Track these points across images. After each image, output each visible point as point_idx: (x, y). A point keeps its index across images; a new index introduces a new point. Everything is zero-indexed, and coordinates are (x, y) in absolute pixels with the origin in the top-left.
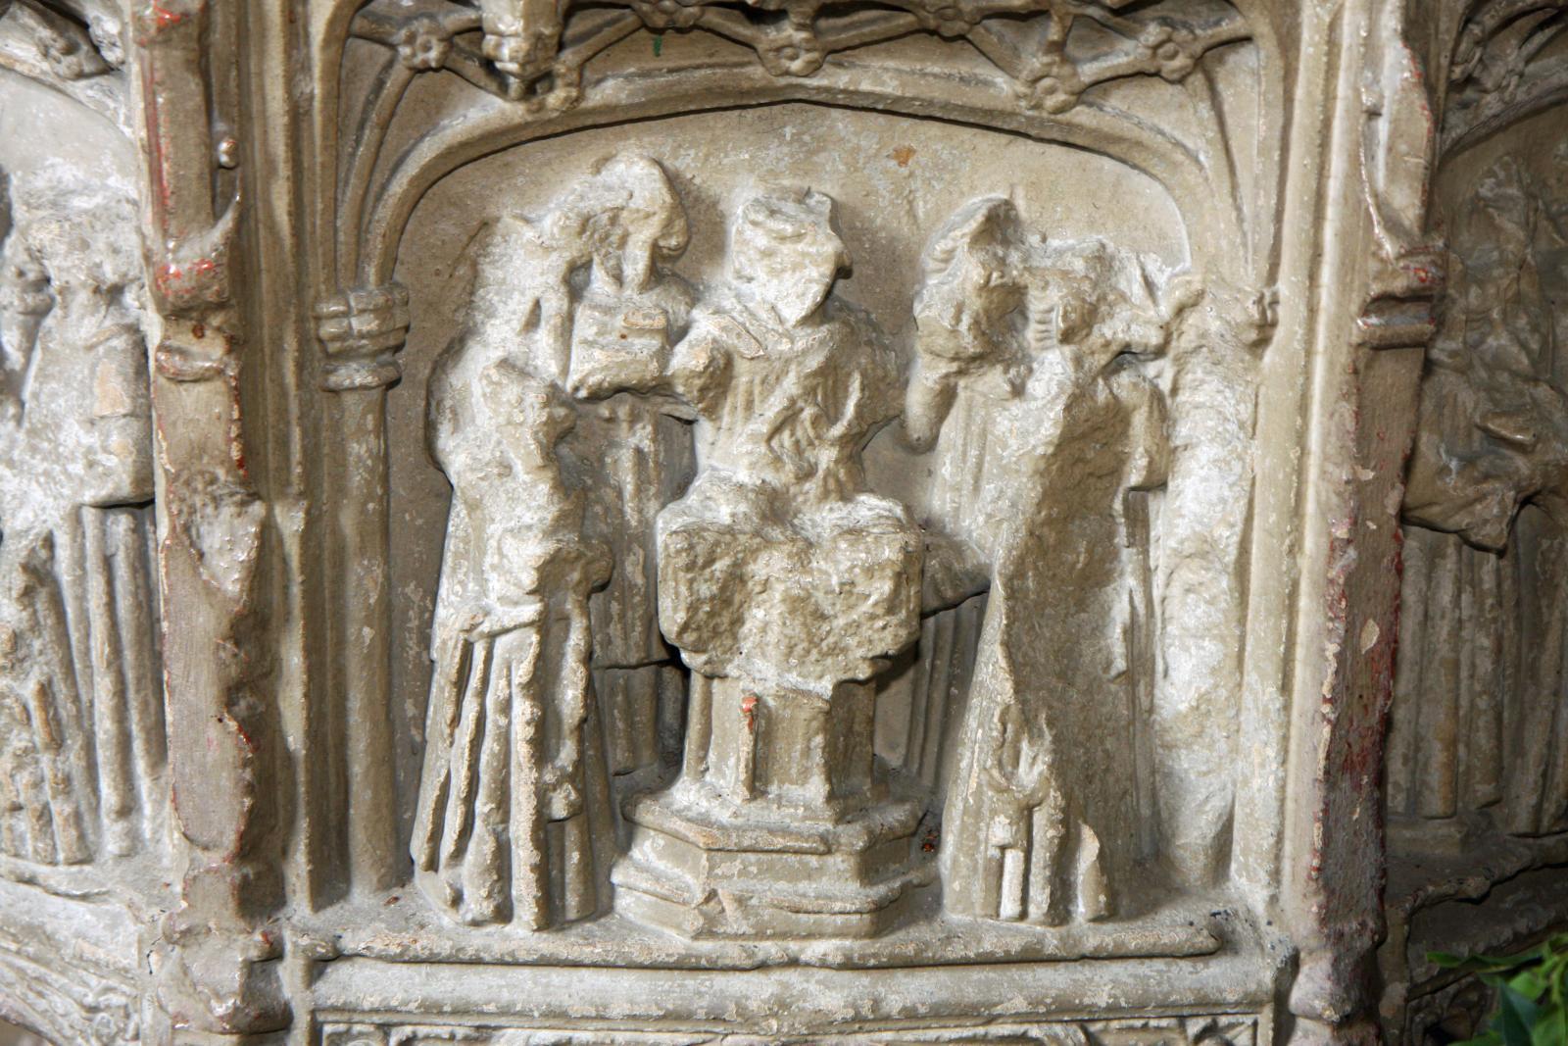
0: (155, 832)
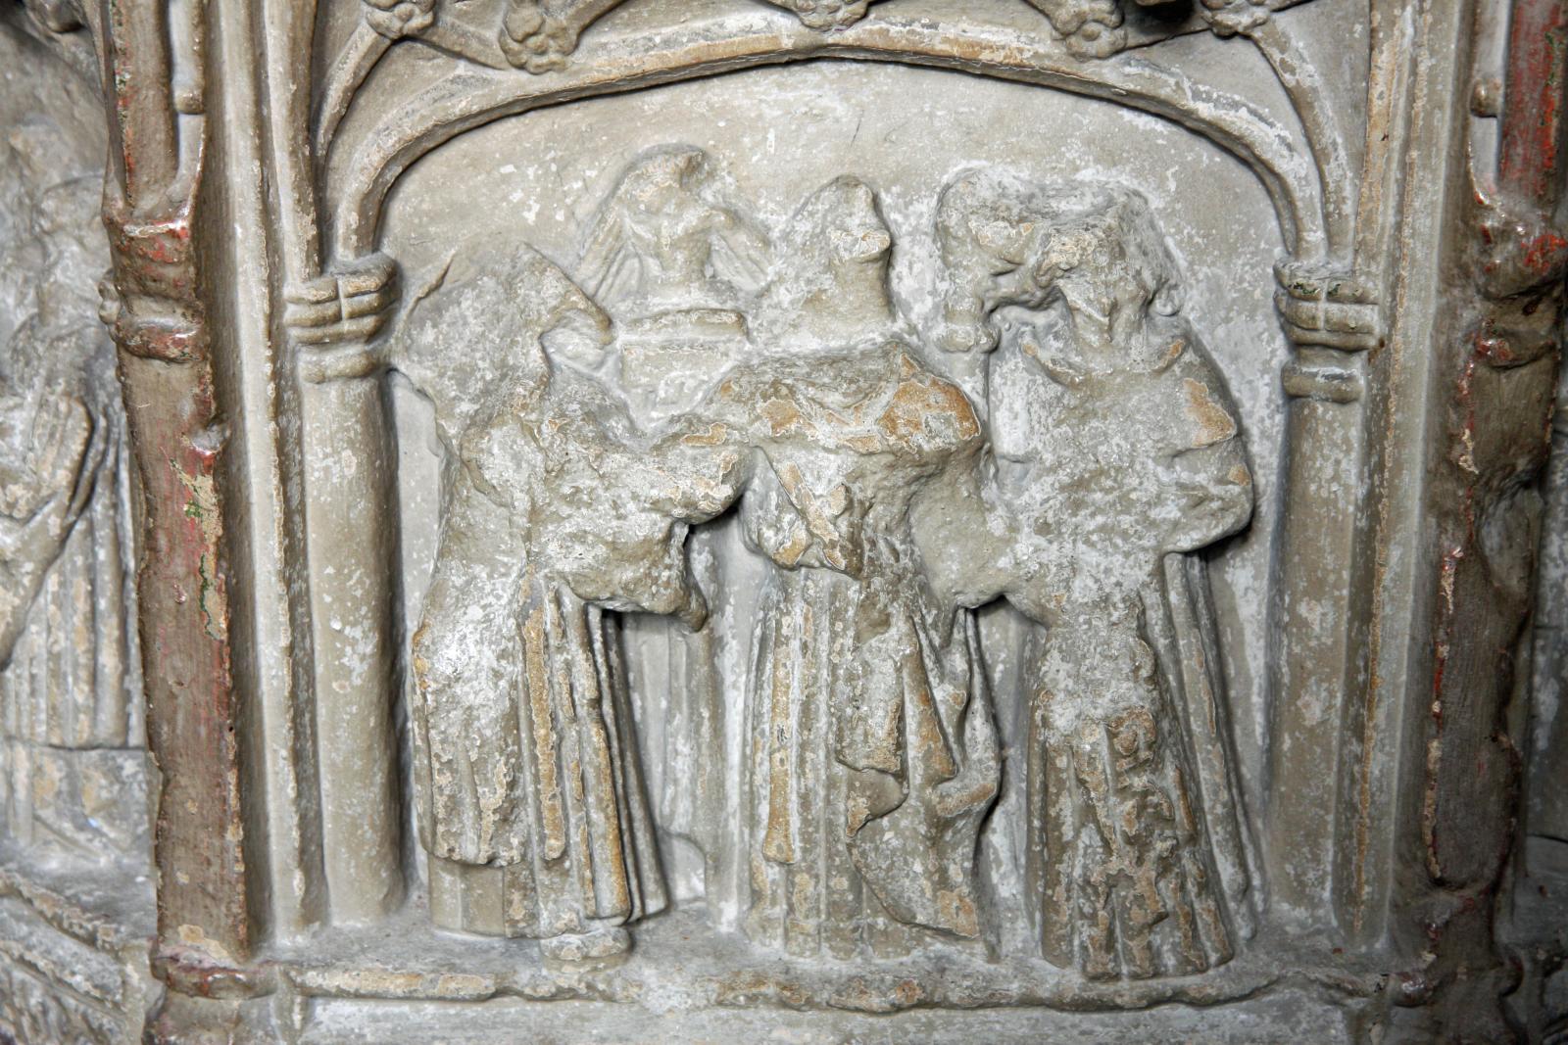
0: (1265, 901)
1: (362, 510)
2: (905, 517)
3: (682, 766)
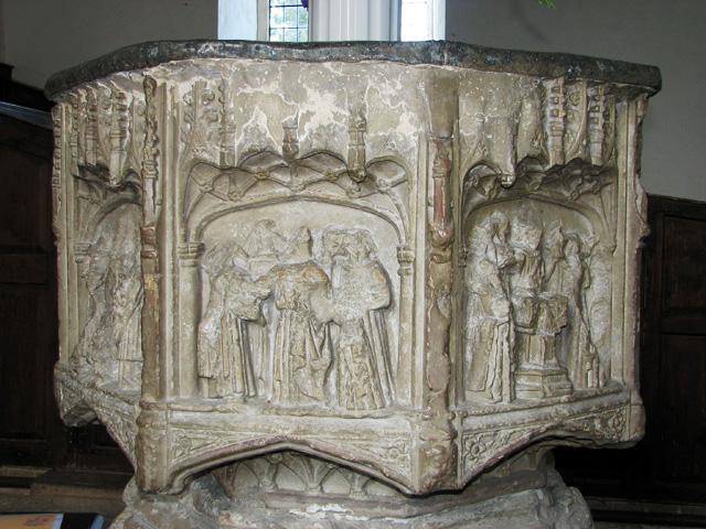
1: (191, 297)
2: (309, 299)
3: (260, 360)
